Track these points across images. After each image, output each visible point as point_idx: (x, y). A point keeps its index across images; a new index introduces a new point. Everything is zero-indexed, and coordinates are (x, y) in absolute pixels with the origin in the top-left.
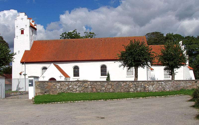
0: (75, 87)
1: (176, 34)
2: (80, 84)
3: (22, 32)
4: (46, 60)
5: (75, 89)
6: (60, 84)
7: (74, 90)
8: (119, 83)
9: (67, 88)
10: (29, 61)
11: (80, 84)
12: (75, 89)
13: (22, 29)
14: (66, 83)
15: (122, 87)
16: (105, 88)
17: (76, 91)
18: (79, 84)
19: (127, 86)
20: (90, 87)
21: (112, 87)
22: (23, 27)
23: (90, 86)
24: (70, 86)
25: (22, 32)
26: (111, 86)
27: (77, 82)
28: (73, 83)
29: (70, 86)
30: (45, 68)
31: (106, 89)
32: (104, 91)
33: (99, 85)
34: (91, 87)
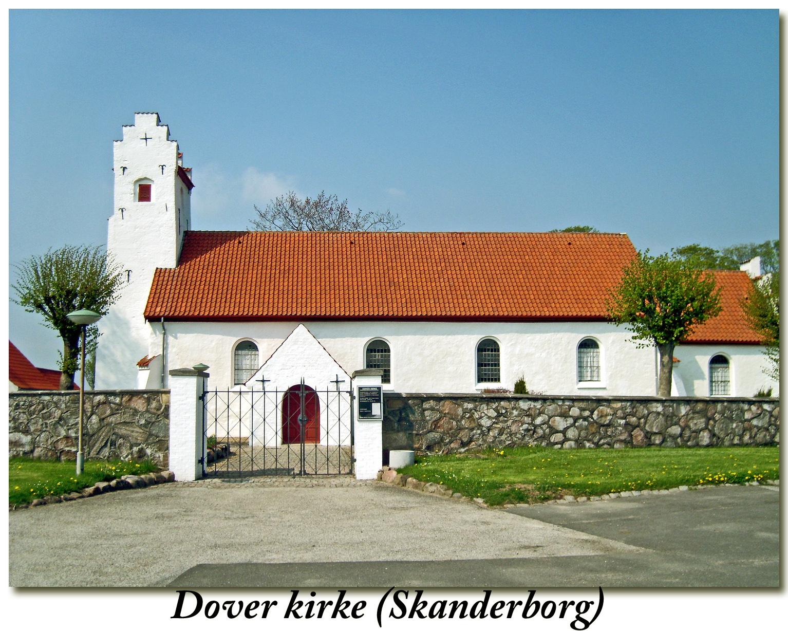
0: (560, 423)
1: (745, 272)
2: (582, 410)
3: (144, 193)
4: (778, 49)
5: (560, 432)
6: (496, 410)
7: (554, 436)
8: (734, 406)
9: (525, 426)
10: (182, 311)
11: (582, 410)
12: (560, 432)
13: (146, 179)
14: (524, 405)
15: (746, 424)
16: (683, 429)
17: (566, 439)
18: (575, 411)
19: (767, 419)
20: (623, 422)
21: (707, 424)
22: (149, 171)
23: (619, 421)
24: (538, 421)
25: (144, 193)
26: (703, 420)
27: (567, 403)
28: (551, 408)
29: (538, 421)
30: (247, 346)
31: (687, 433)
32: (679, 440)
33: (659, 413)
34: (627, 424)
